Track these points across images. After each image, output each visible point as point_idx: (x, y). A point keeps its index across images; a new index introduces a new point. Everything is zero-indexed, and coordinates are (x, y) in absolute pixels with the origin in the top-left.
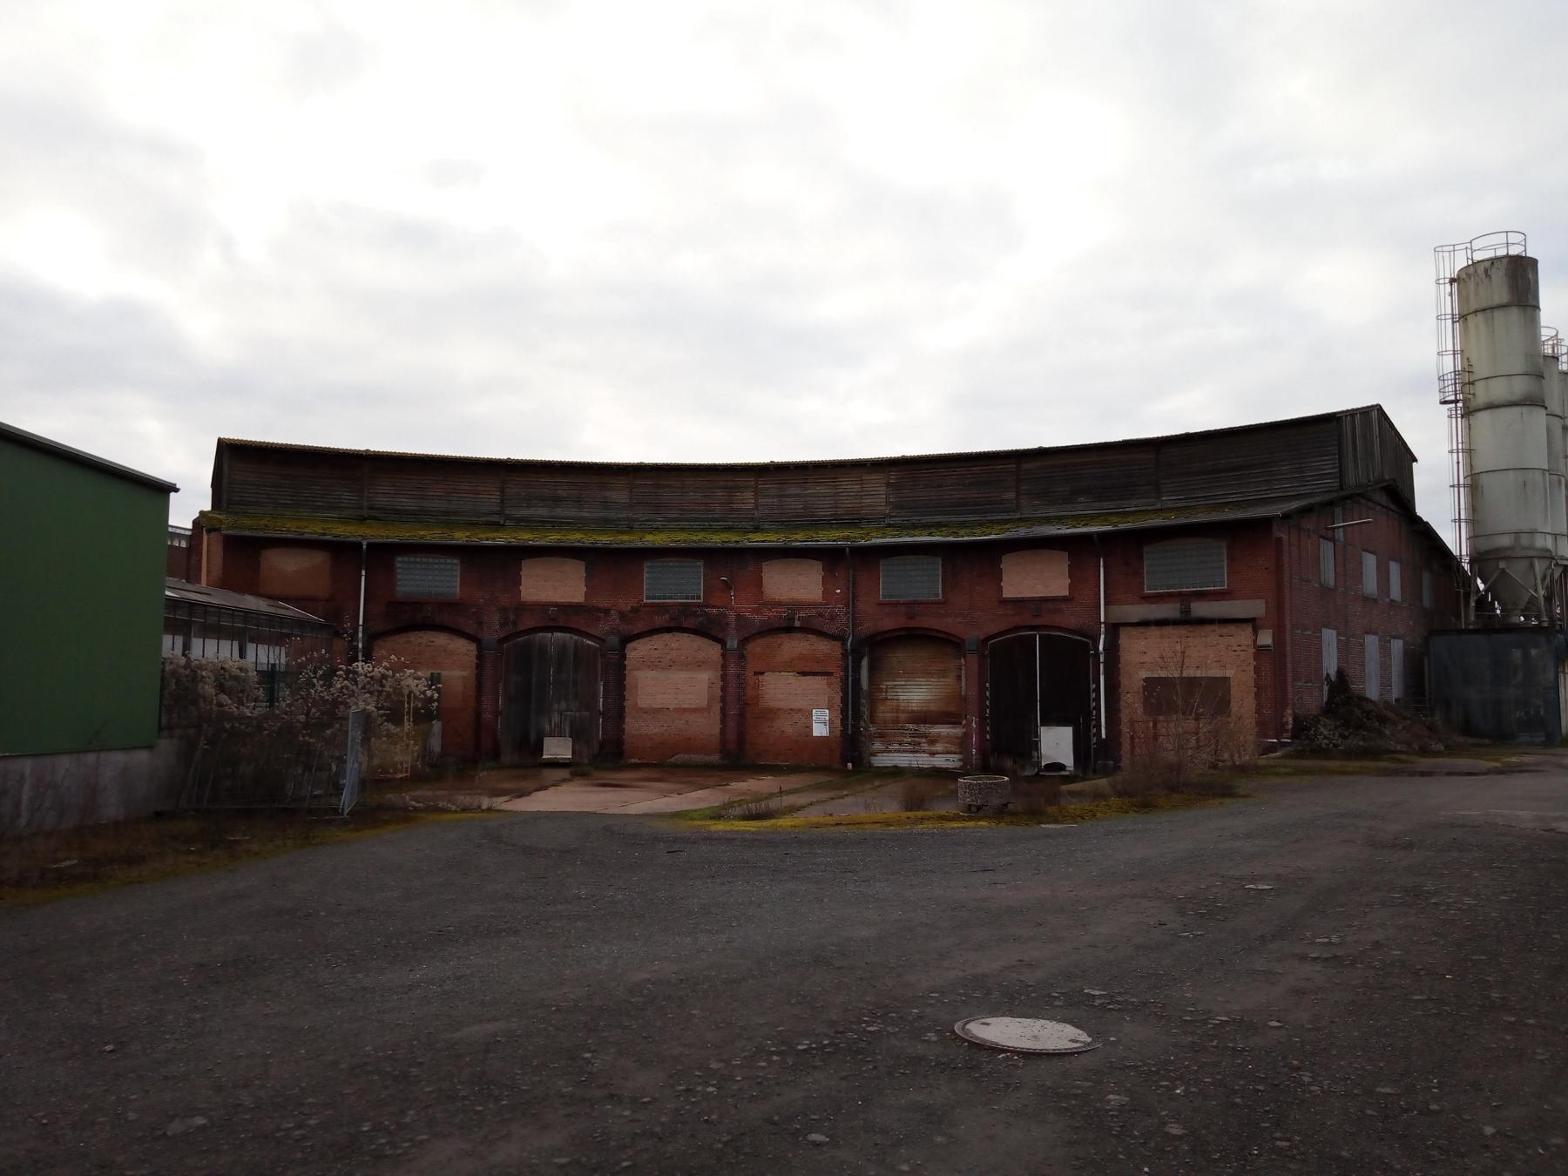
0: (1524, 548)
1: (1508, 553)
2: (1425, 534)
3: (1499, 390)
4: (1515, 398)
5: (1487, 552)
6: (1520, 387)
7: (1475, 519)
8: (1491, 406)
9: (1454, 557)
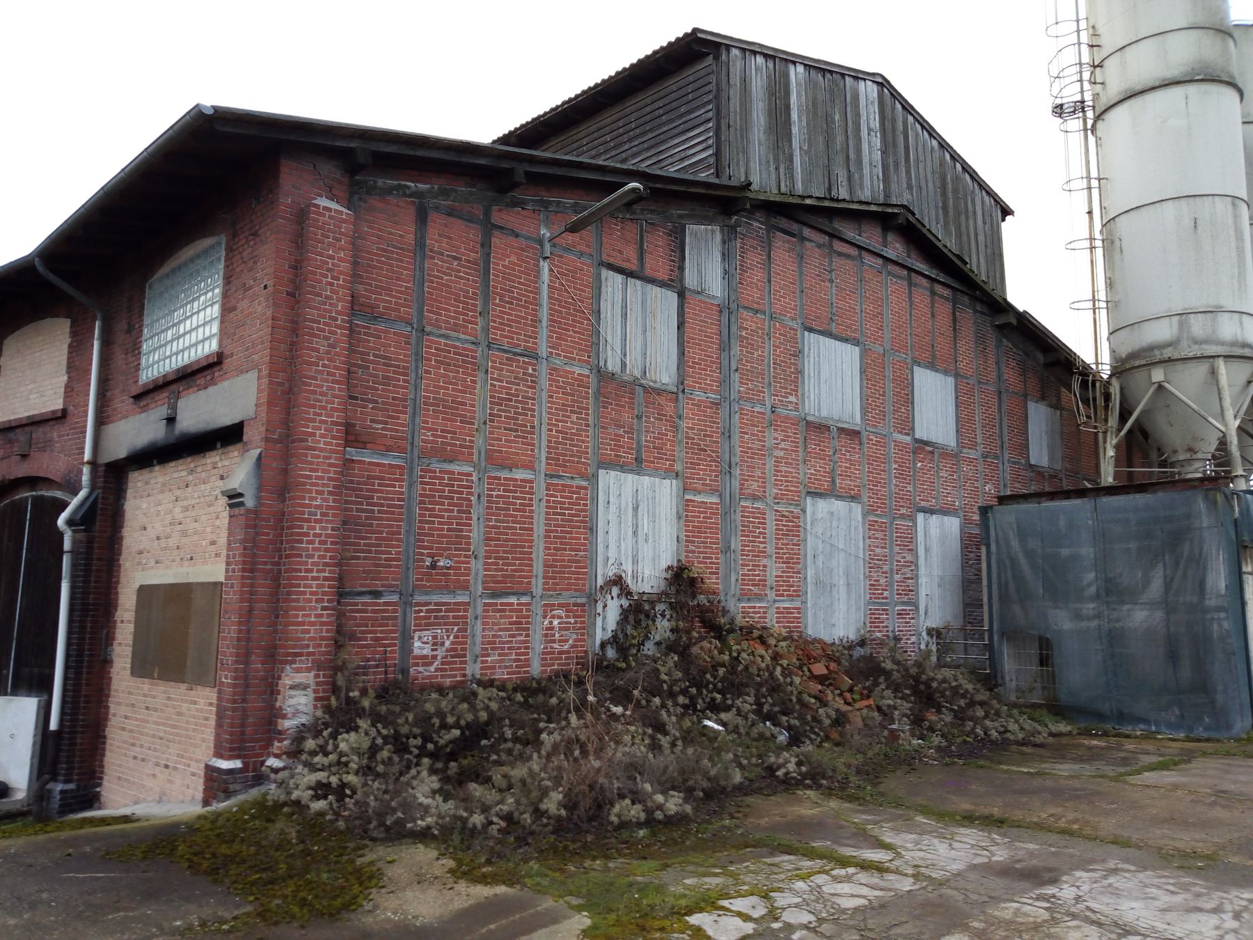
0: (1196, 342)
1: (1168, 353)
2: (1028, 336)
3: (1144, 65)
4: (1174, 72)
5: (1133, 356)
6: (1183, 52)
7: (1115, 298)
8: (641, 258)
9: (1086, 367)
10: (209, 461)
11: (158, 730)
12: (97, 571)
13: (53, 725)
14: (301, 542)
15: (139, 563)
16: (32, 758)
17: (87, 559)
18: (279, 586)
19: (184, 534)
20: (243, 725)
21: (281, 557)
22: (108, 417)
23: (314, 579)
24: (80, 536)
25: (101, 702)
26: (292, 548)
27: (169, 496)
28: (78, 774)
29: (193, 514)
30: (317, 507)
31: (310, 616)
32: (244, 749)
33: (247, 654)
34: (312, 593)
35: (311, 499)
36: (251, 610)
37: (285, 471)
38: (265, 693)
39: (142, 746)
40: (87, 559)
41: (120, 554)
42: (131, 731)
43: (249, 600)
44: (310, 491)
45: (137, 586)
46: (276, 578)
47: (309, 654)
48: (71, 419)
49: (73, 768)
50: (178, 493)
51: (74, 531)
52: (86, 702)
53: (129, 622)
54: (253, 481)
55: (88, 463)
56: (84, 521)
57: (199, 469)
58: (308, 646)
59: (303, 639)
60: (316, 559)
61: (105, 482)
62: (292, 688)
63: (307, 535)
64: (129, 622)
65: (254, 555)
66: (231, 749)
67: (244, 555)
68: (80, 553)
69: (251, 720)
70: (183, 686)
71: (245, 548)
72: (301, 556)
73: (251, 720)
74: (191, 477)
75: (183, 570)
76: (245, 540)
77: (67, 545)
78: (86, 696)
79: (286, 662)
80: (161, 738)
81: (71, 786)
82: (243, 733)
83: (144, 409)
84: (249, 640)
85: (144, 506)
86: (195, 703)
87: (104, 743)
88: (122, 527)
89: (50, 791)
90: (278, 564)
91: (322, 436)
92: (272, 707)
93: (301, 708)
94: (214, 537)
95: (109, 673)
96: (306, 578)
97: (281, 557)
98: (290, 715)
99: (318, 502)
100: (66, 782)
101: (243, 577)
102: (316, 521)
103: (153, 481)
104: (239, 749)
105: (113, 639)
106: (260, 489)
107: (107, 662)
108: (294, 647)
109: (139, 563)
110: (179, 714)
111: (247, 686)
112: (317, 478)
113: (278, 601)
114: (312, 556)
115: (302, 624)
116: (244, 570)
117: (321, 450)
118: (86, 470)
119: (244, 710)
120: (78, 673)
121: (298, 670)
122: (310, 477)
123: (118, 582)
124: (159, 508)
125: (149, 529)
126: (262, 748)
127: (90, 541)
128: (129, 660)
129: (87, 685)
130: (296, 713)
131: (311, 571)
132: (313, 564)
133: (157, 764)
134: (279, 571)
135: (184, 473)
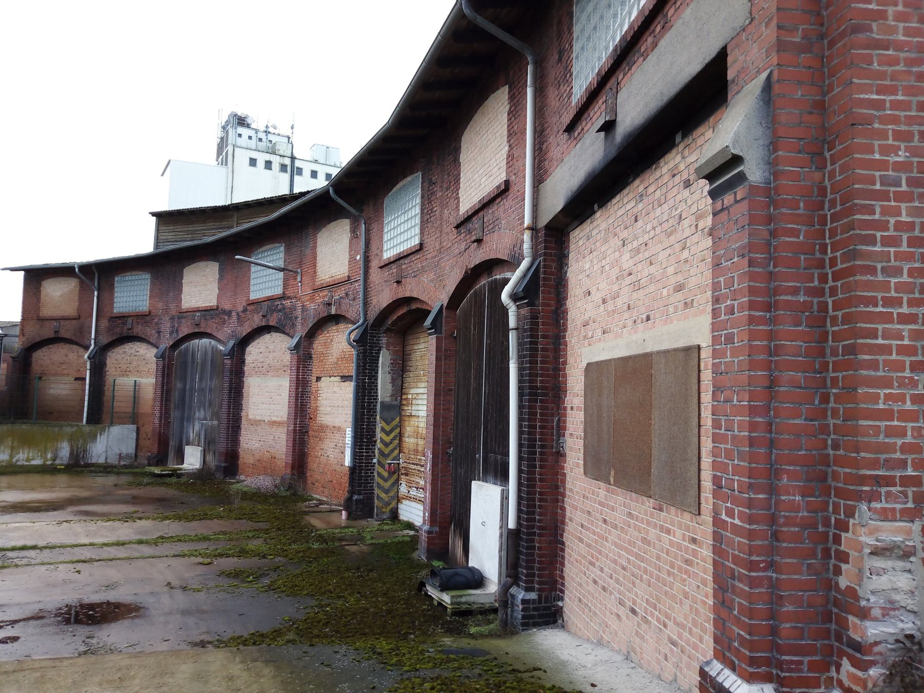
10: (665, 170)
11: (620, 556)
12: (543, 349)
13: (512, 524)
14: (872, 241)
15: (585, 337)
16: (500, 550)
17: (531, 336)
18: (824, 337)
19: (637, 286)
20: (772, 615)
21: (823, 279)
22: (546, 172)
23: (904, 319)
24: (525, 311)
25: (557, 501)
26: (855, 254)
27: (616, 242)
28: (539, 583)
29: (647, 254)
30: (898, 167)
31: (902, 398)
32: (780, 665)
33: (773, 473)
34: (902, 350)
35: (885, 150)
36: (772, 383)
37: (821, 107)
38: (813, 555)
39: (602, 570)
40: (531, 336)
41: (565, 330)
42: (589, 546)
43: (768, 365)
44: (883, 135)
45: (584, 365)
46: (819, 321)
47: (906, 481)
48: (514, 189)
49: (533, 575)
50: (624, 234)
51: (518, 307)
52: (540, 500)
53: (579, 408)
54: (759, 131)
55: (528, 228)
56: (527, 294)
57: (651, 189)
58: (903, 464)
59: (891, 448)
60: (905, 278)
61: (546, 248)
62: (875, 552)
63: (884, 226)
64: (579, 408)
65: (771, 276)
66: (752, 662)
67: (752, 277)
68: (525, 331)
69: (788, 608)
70: (650, 503)
71: (751, 263)
72: (872, 270)
73: (788, 608)
74: (640, 206)
75: (638, 336)
76: (751, 247)
77: (512, 322)
78: (541, 493)
79: (859, 497)
80: (624, 569)
81: (533, 596)
82: (774, 631)
83: (578, 140)
84: (772, 444)
85: (587, 266)
86: (668, 532)
87: (563, 550)
88: (566, 298)
89: (513, 596)
90: (820, 292)
91: (900, 17)
92: (830, 585)
93: (900, 598)
94: (680, 278)
95: (563, 468)
96: (887, 318)
97: (823, 279)
98: (876, 612)
99: (902, 156)
100: (527, 590)
101: (751, 320)
102: (900, 197)
103: (595, 232)
104: (768, 662)
105: (565, 428)
106: (773, 145)
107: (560, 455)
108: (875, 464)
109: (585, 337)
110: (644, 540)
111: (776, 536)
112: (896, 105)
113: (825, 367)
114: (898, 271)
115: (888, 415)
116: (752, 306)
117: (899, 46)
118: (527, 236)
119: (774, 585)
120: (531, 472)
121: (886, 515)
122: (879, 105)
123: (565, 363)
124: (604, 263)
125: (593, 293)
126: (812, 666)
127: (534, 317)
128: (581, 455)
129: (541, 480)
130: (890, 609)
131: (898, 302)
132: (899, 287)
133: (621, 603)
134: (823, 307)
135: (632, 204)
